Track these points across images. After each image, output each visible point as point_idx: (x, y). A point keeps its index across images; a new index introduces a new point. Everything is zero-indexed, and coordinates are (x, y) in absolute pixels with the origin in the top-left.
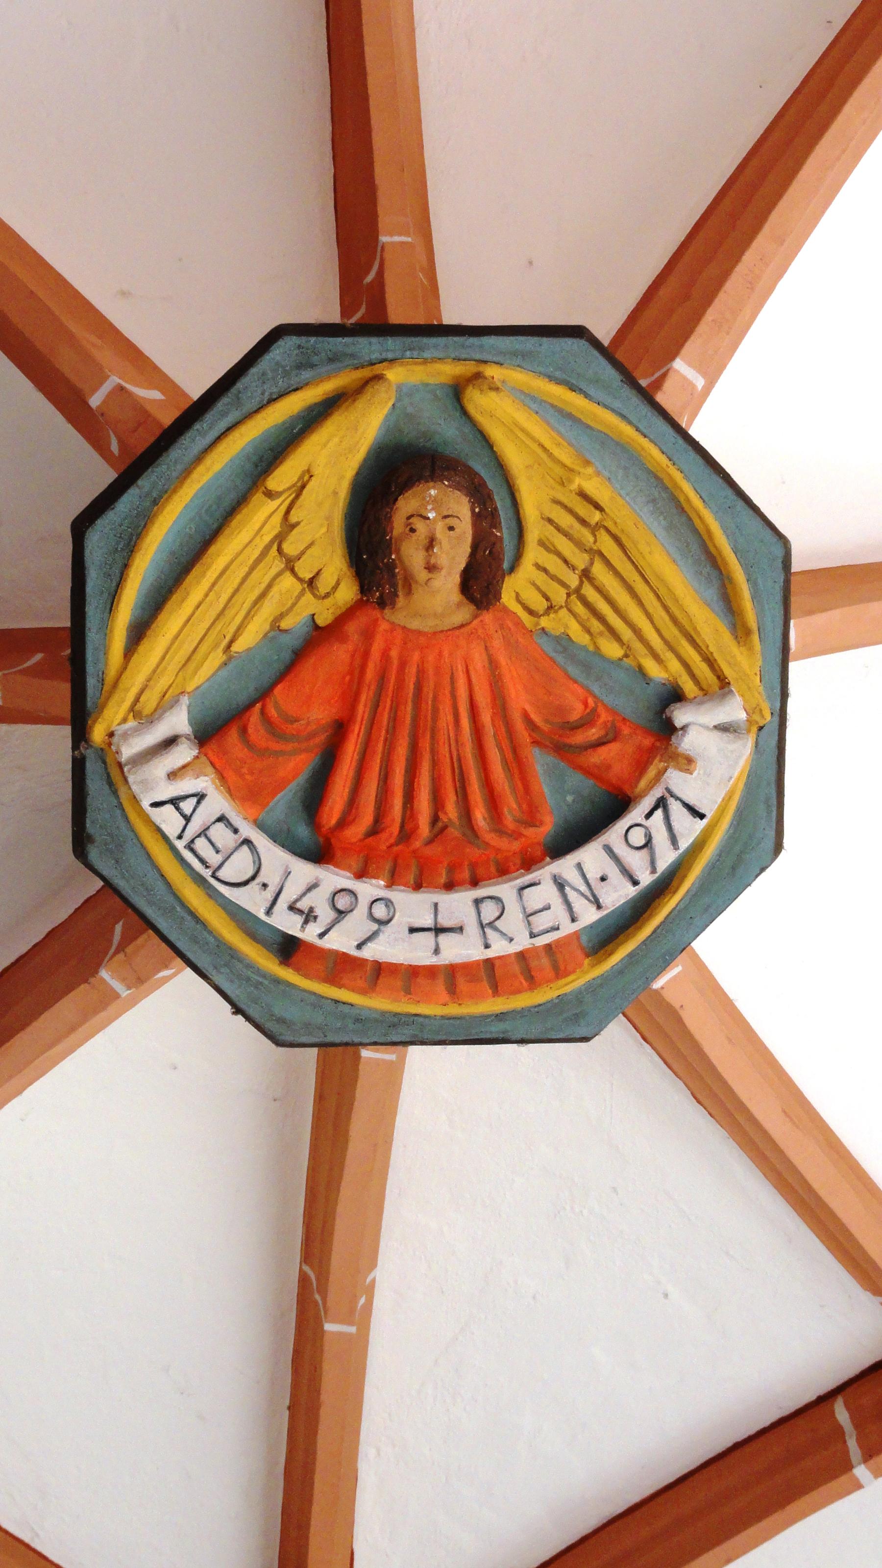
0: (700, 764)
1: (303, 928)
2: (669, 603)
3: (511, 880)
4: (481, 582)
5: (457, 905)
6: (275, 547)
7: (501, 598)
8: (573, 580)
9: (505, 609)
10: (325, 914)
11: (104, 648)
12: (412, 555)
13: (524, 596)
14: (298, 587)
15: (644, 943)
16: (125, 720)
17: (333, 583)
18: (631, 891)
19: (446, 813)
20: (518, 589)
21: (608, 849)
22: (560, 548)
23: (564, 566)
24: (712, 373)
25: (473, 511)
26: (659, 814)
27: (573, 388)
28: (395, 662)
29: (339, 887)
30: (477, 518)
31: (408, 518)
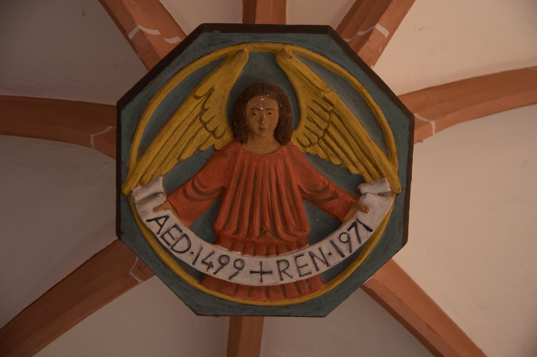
0: (370, 212)
2: (360, 144)
5: (270, 262)
6: (199, 118)
8: (321, 133)
9: (293, 145)
10: (216, 265)
11: (129, 157)
13: (300, 139)
14: (208, 134)
15: (347, 279)
16: (137, 186)
19: (266, 226)
20: (299, 136)
21: (332, 242)
24: (393, 29)
25: (279, 106)
26: (353, 229)
27: (322, 55)
28: (246, 166)
29: (222, 254)
30: (281, 110)
31: (252, 109)
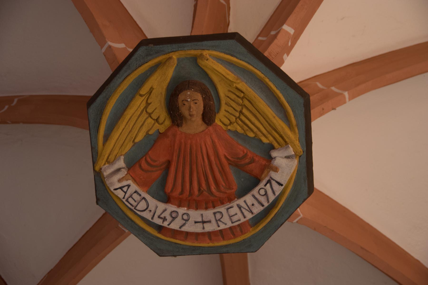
0: (280, 169)
1: (163, 223)
3: (224, 206)
4: (208, 117)
5: (209, 214)
7: (215, 121)
8: (237, 114)
10: (169, 219)
12: (184, 111)
13: (222, 120)
14: (153, 122)
15: (269, 223)
16: (105, 164)
17: (163, 120)
18: (262, 208)
20: (221, 118)
21: (254, 196)
22: (232, 105)
23: (234, 111)
25: (202, 97)
26: (268, 185)
29: (172, 210)
30: (204, 99)
31: (183, 101)
